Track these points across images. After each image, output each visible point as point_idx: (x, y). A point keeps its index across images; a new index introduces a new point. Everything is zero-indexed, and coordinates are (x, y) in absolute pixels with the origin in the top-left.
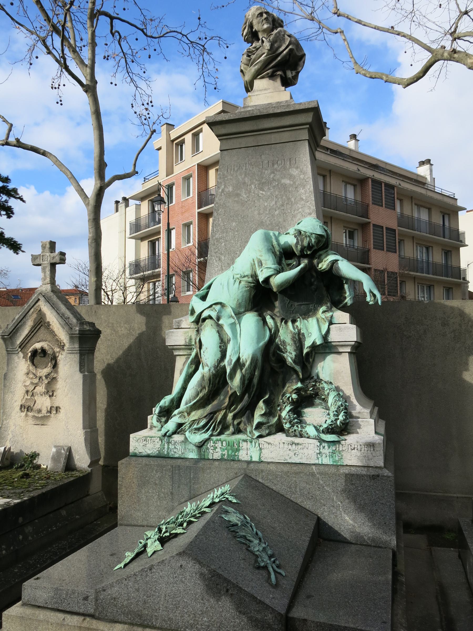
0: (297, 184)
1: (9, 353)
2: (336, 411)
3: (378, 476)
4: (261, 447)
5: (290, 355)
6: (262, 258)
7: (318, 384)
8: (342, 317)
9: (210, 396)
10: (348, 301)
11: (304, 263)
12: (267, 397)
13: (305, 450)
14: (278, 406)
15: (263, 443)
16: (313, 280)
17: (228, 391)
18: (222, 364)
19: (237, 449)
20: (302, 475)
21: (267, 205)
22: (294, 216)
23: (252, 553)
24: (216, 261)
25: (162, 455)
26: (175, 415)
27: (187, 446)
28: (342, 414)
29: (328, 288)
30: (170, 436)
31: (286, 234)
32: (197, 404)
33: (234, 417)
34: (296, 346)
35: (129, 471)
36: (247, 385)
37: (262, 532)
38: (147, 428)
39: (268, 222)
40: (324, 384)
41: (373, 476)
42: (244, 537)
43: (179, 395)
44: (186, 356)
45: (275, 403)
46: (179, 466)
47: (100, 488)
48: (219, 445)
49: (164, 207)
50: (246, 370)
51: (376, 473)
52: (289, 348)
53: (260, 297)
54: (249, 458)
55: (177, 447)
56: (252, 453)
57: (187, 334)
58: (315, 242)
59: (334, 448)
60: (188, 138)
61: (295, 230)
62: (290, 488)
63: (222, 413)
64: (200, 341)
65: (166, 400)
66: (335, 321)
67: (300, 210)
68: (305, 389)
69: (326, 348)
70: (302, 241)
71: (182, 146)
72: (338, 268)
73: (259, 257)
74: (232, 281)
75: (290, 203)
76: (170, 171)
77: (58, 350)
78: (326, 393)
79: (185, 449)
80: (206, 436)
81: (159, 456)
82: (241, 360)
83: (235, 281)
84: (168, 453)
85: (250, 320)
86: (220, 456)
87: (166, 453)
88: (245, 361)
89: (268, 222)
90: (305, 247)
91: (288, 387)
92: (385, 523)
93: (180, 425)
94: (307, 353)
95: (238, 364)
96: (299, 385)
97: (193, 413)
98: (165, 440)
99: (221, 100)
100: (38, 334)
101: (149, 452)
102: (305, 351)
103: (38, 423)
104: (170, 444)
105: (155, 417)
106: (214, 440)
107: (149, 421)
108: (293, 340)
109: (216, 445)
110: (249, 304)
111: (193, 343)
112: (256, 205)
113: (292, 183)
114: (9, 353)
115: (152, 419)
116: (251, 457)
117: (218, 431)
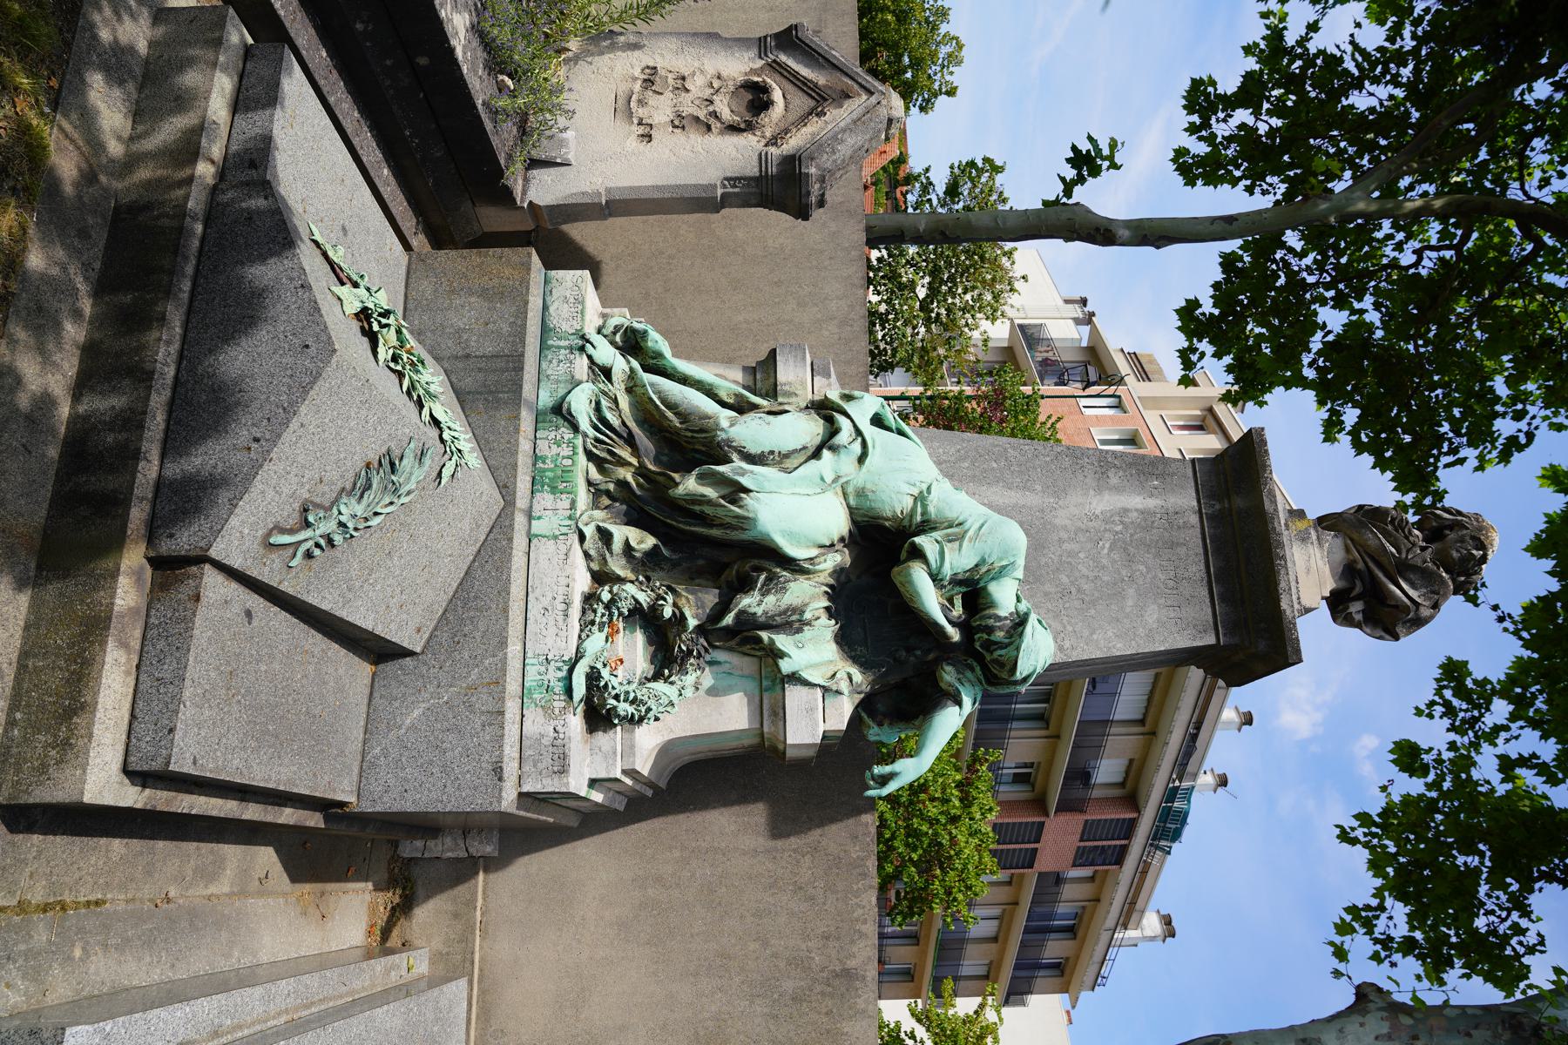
1: (762, 45)
2: (635, 698)
3: (500, 779)
8: (840, 714)
10: (874, 733)
12: (665, 552)
13: (552, 630)
14: (648, 579)
18: (735, 456)
20: (502, 621)
22: (1057, 616)
23: (336, 501)
28: (631, 709)
29: (903, 686)
32: (650, 407)
36: (690, 509)
37: (380, 527)
39: (1043, 561)
42: (368, 487)
45: (654, 570)
47: (486, 229)
48: (567, 451)
51: (506, 775)
52: (770, 600)
59: (557, 690)
62: (476, 597)
67: (1070, 628)
69: (772, 681)
77: (768, 134)
79: (558, 381)
80: (585, 425)
84: (549, 347)
87: (550, 342)
89: (1043, 561)
93: (607, 372)
94: (760, 640)
95: (736, 491)
100: (800, 94)
101: (552, 309)
102: (764, 635)
103: (620, 102)
111: (780, 400)
114: (762, 45)
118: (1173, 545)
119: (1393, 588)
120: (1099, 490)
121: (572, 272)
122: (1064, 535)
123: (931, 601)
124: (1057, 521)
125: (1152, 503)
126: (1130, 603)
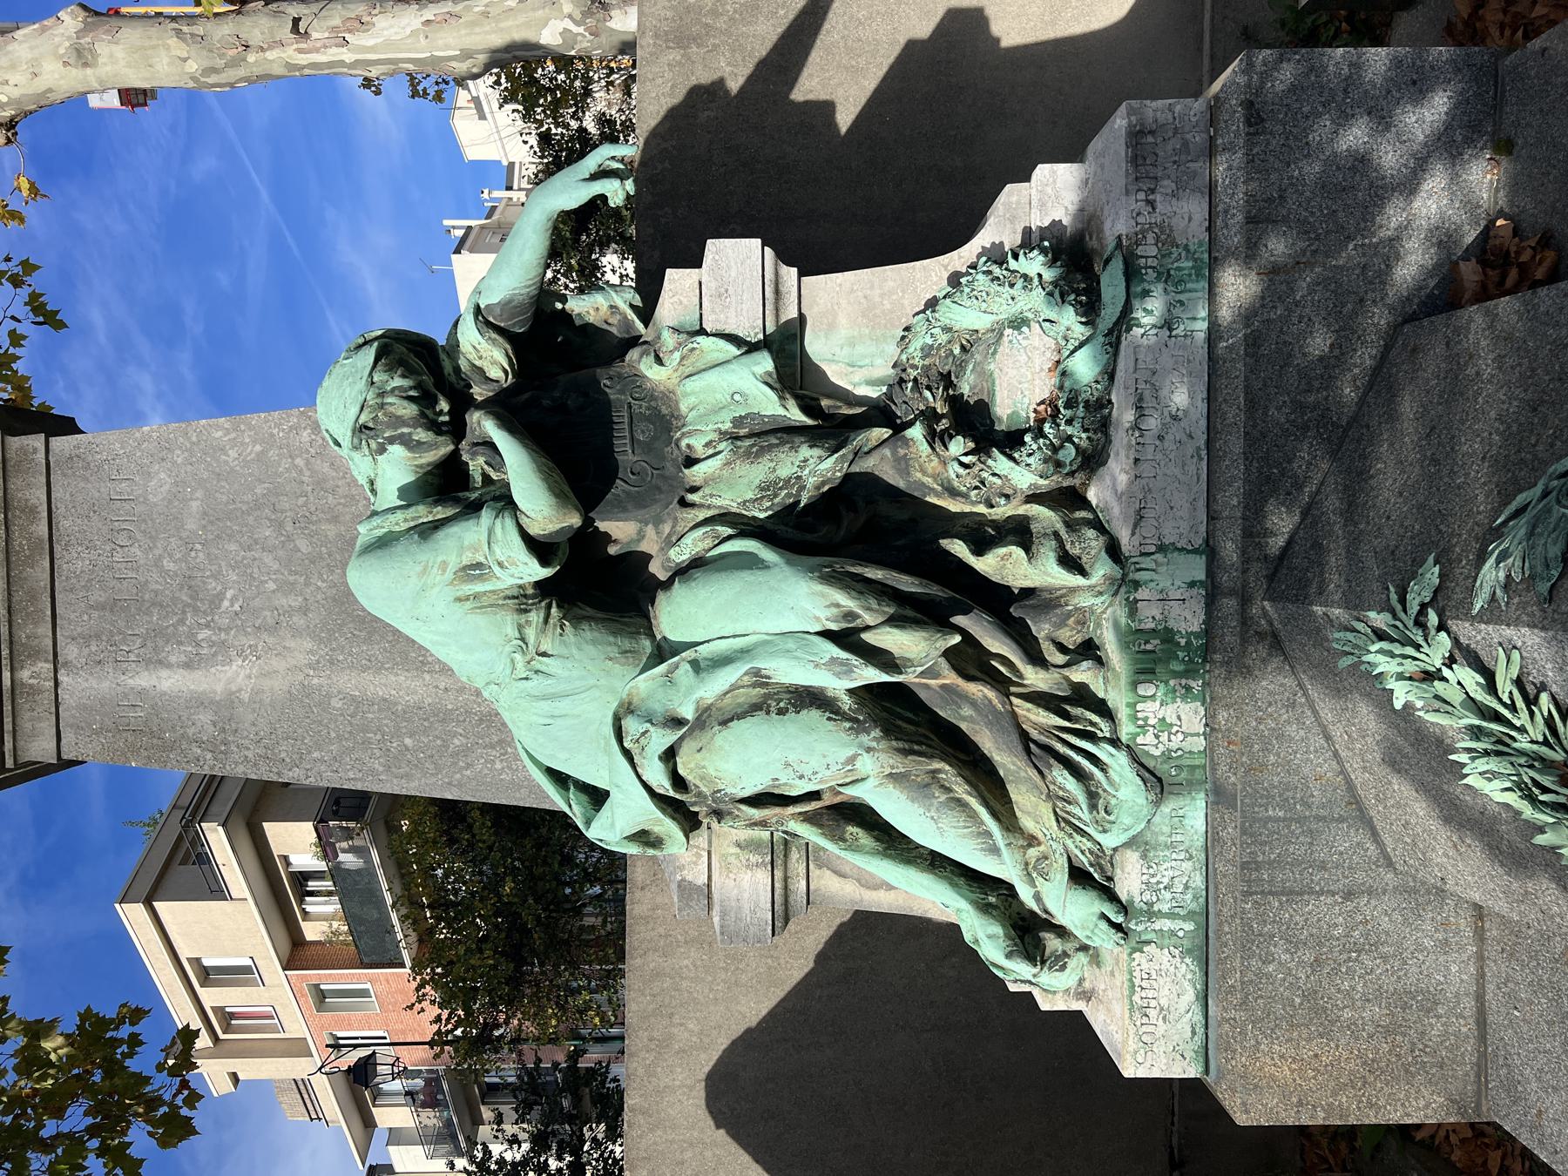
4: (1153, 549)
5: (814, 469)
6: (454, 562)
7: (913, 373)
9: (962, 756)
11: (486, 426)
15: (1136, 540)
16: (546, 402)
17: (943, 687)
18: (846, 703)
19: (1163, 642)
20: (1258, 385)
21: (275, 581)
24: (468, 766)
25: (1200, 940)
26: (1038, 897)
27: (1162, 839)
30: (1124, 909)
31: (373, 491)
32: (998, 807)
33: (1038, 660)
34: (777, 445)
35: (1272, 1077)
38: (1079, 1014)
40: (911, 350)
41: (1248, 123)
43: (961, 881)
44: (811, 866)
46: (1244, 866)
49: (385, 1055)
50: (869, 609)
52: (785, 471)
53: (596, 588)
54: (1195, 591)
55: (1166, 881)
56: (1178, 583)
57: (732, 859)
58: (403, 376)
60: (211, 997)
61: (356, 448)
63: (1024, 709)
64: (758, 800)
65: (981, 935)
66: (691, 320)
67: (299, 461)
68: (929, 417)
70: (398, 421)
71: (232, 1016)
72: (505, 304)
73: (449, 575)
74: (536, 684)
75: (273, 499)
76: (298, 1048)
78: (943, 338)
79: (1172, 846)
81: (1203, 953)
82: (834, 627)
83: (537, 672)
84: (1190, 916)
85: (677, 615)
86: (1193, 705)
87: (1189, 926)
88: (835, 611)
90: (422, 415)
91: (924, 472)
92: (1414, 83)
93: (1079, 876)
96: (916, 432)
97: (1027, 823)
98: (1140, 928)
99: (133, 916)
101: (1190, 995)
102: (796, 416)
104: (1156, 908)
105: (1047, 978)
106: (1132, 729)
107: (1061, 1005)
108: (758, 455)
109: (1152, 721)
110: (625, 624)
112: (271, 621)
113: (199, 494)
115: (1053, 990)
116: (1192, 585)
117: (1095, 718)
118: (112, 606)
120: (230, 701)
121: (1156, 1074)
122: (299, 621)
123: (518, 467)
124: (308, 644)
125: (143, 680)
126: (195, 505)
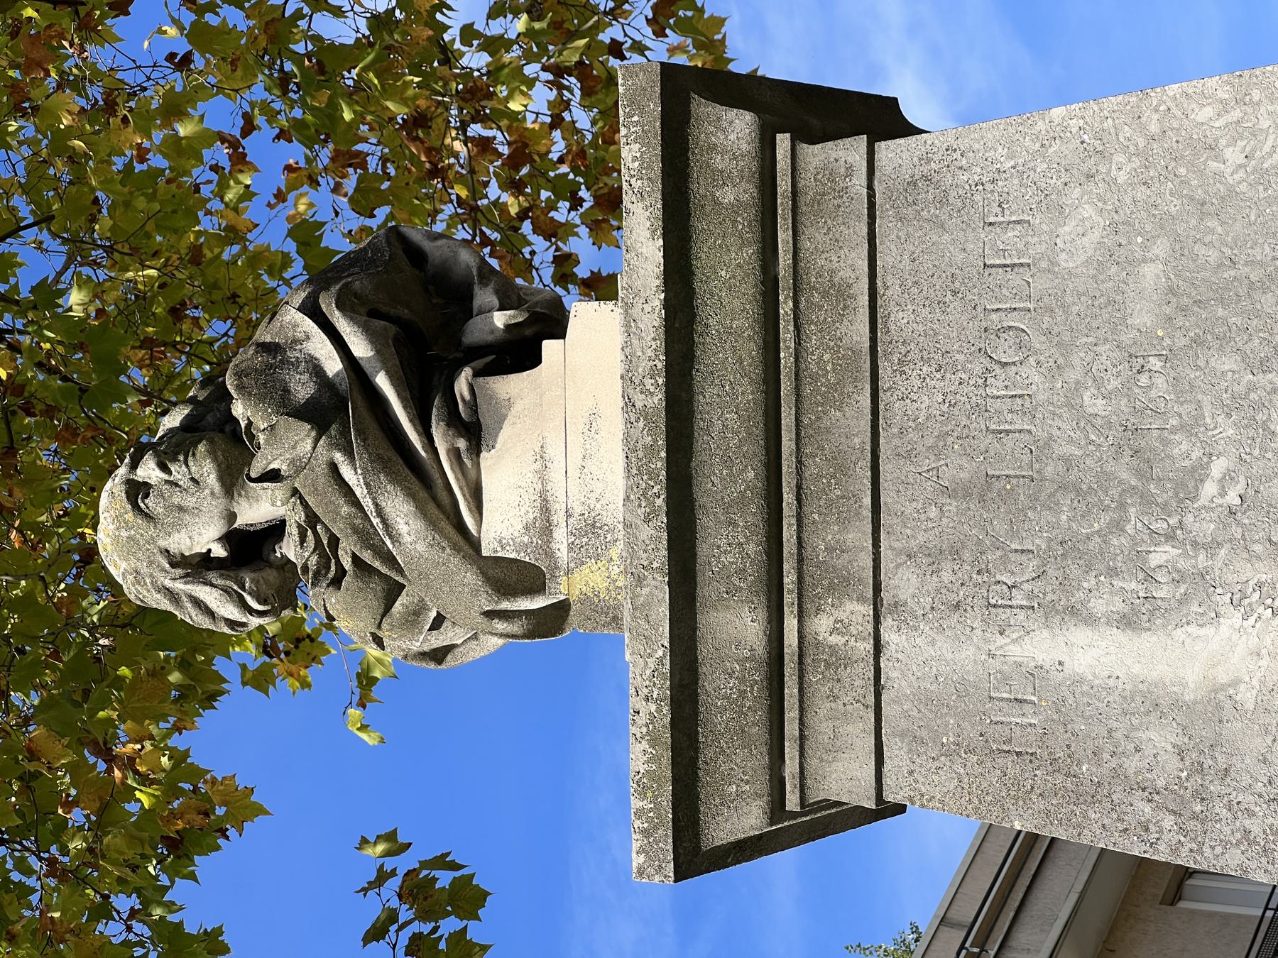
0: (1174, 207)
118: (983, 490)
119: (361, 348)
120: (1217, 704)
125: (1040, 647)
126: (1151, 273)
